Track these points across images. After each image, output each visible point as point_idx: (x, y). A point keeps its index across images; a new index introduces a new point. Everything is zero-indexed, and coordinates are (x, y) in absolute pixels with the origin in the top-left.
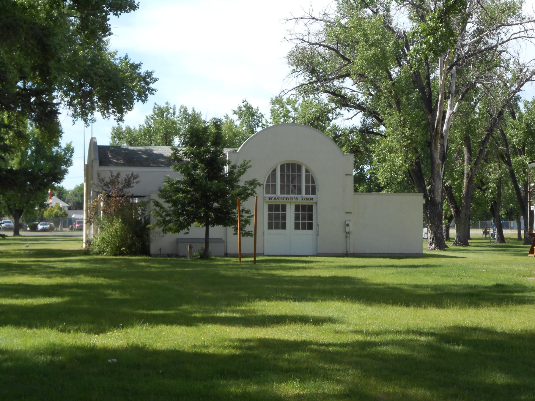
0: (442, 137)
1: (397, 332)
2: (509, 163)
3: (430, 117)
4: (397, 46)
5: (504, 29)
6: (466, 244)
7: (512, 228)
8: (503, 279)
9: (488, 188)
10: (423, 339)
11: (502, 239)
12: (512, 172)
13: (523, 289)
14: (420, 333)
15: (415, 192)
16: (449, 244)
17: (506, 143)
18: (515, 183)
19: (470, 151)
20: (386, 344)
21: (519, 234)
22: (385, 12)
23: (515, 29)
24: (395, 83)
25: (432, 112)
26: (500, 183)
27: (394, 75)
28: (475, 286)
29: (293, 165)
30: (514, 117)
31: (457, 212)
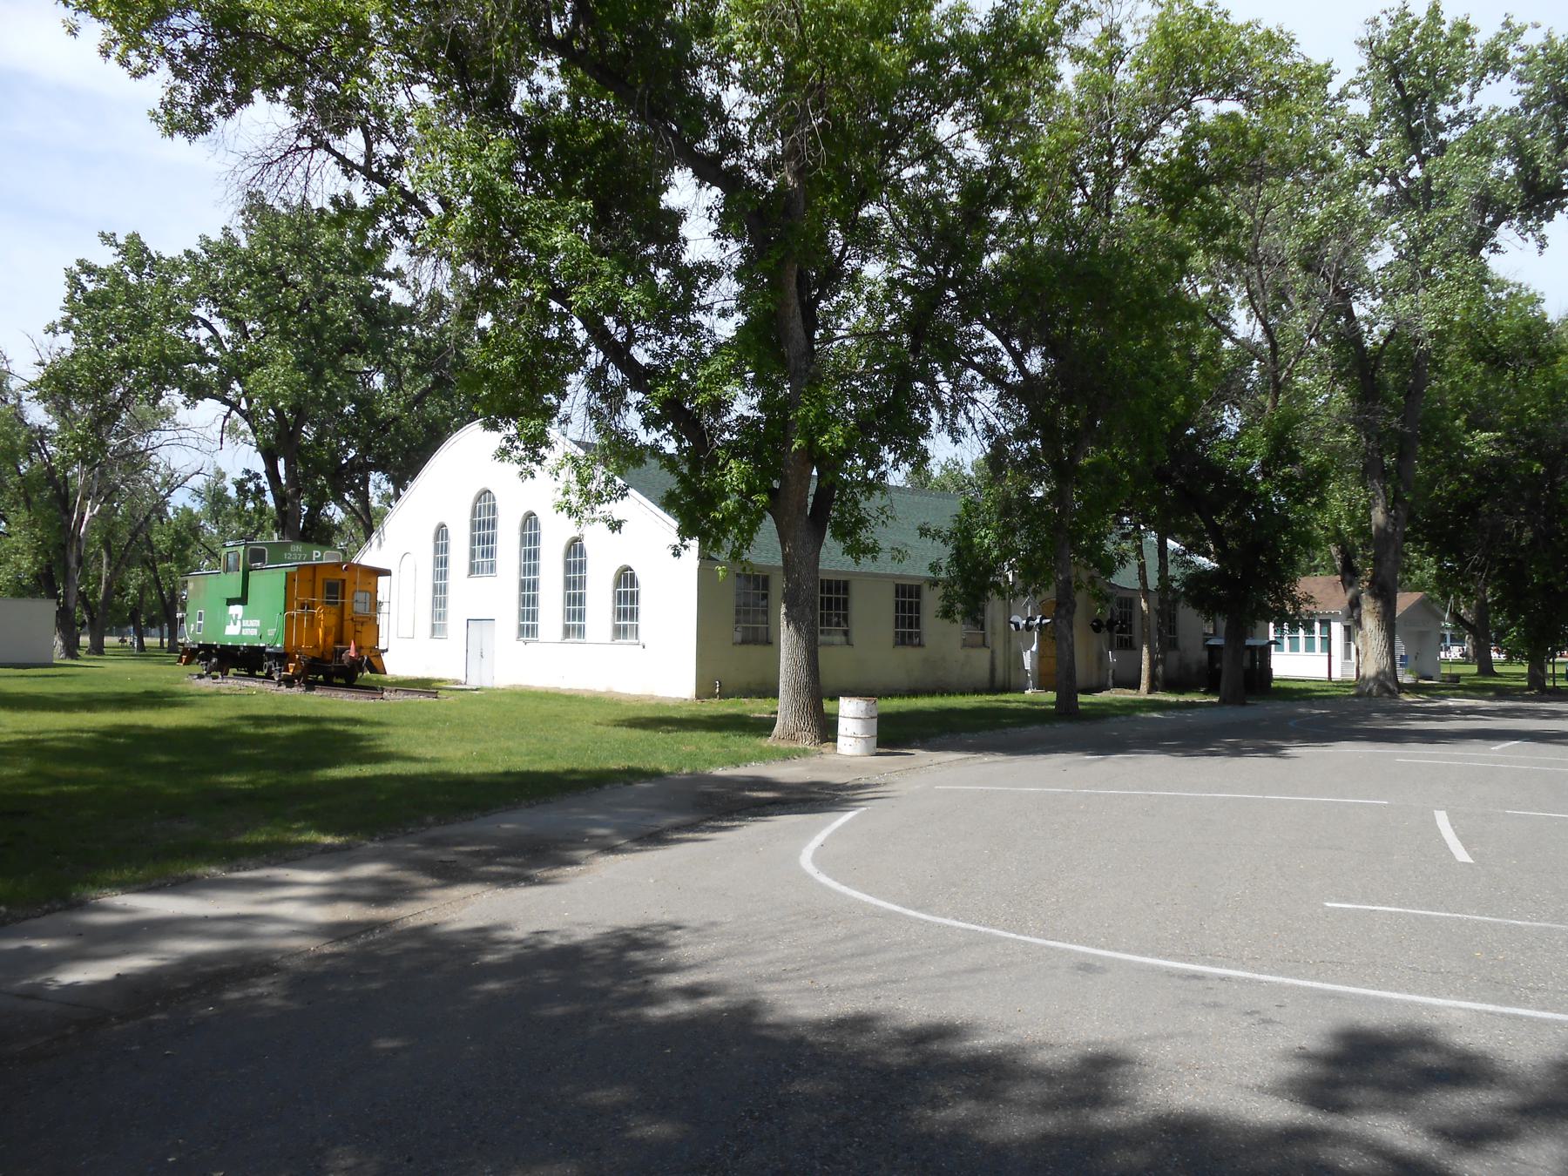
0: (79, 539)
1: (59, 731)
2: (154, 569)
3: (65, 518)
4: (30, 439)
5: (155, 433)
6: (102, 653)
7: (152, 636)
8: (152, 686)
9: (128, 595)
10: (85, 735)
11: (142, 647)
12: (157, 578)
13: (174, 694)
14: (82, 731)
15: (43, 597)
16: (81, 653)
17: (151, 547)
18: (161, 590)
19: (110, 555)
20: (52, 740)
21: (162, 642)
22: (16, 402)
23: (168, 435)
24: (25, 480)
25: (70, 513)
26: (142, 589)
27: (23, 471)
28: (123, 694)
29: (838, 582)
30: (162, 523)
31: (92, 619)
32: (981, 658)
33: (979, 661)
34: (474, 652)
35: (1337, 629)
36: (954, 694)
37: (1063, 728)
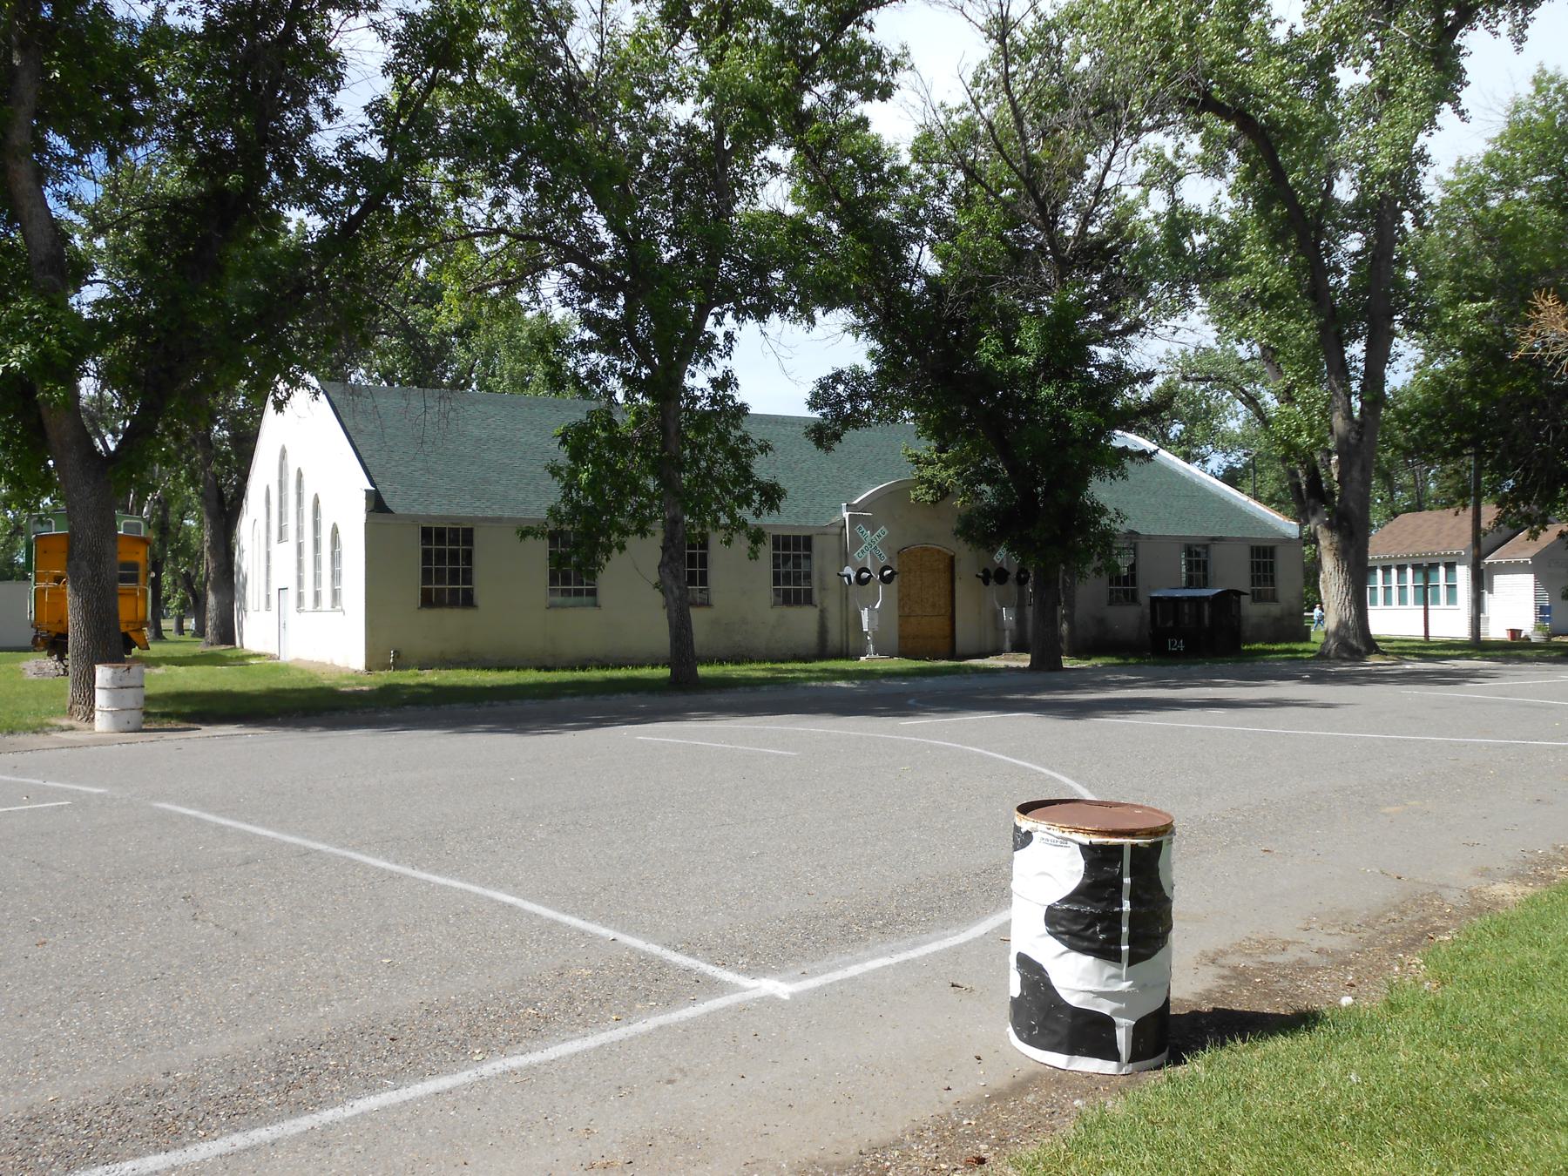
29: (797, 538)
32: (802, 623)
33: (802, 623)
34: (282, 626)
35: (1463, 574)
36: (489, 669)
37: (680, 700)
